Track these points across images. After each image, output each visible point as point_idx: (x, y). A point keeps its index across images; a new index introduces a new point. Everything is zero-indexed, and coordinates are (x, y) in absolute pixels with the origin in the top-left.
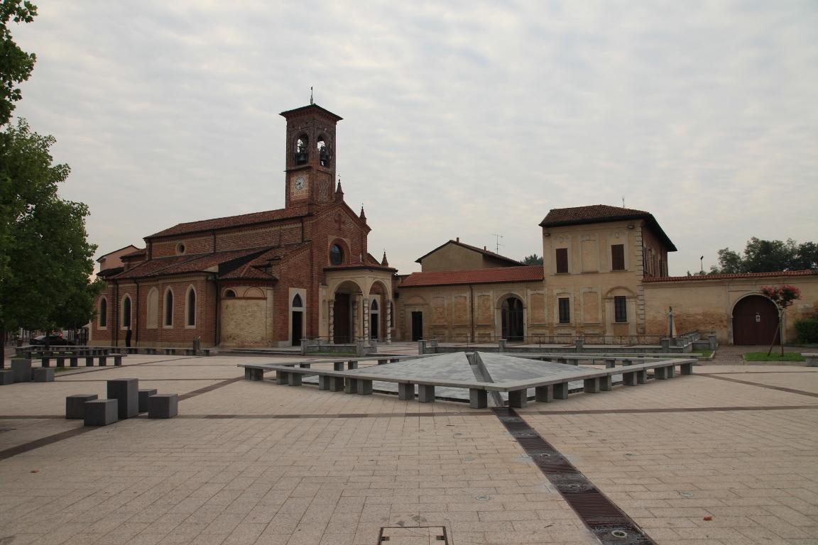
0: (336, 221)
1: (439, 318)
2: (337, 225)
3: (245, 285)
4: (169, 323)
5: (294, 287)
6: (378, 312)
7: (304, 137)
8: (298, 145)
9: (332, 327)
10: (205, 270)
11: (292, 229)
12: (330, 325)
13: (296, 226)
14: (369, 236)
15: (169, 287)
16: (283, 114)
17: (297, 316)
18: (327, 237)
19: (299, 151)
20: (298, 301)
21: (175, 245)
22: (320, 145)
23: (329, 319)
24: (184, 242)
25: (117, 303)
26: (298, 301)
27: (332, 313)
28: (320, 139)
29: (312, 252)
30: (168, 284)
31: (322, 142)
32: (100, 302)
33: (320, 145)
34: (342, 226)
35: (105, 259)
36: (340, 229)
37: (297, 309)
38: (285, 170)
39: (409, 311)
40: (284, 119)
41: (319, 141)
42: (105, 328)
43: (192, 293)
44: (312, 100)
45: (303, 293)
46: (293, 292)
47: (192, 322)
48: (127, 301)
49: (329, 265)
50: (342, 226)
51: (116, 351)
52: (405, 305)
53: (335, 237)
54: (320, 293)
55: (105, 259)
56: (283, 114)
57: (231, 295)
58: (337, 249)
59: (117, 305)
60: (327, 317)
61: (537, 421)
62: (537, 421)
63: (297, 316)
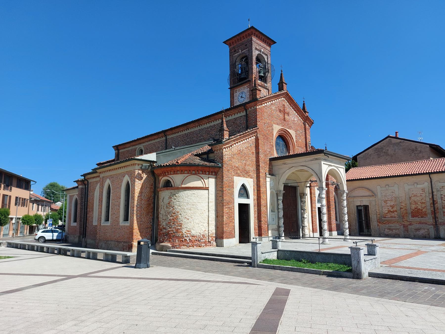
0: (280, 111)
1: (389, 211)
2: (281, 116)
3: (182, 172)
4: (107, 219)
5: (239, 176)
6: (251, 201)
9: (282, 221)
10: (139, 157)
11: (235, 119)
12: (279, 218)
13: (239, 115)
17: (244, 209)
18: (272, 126)
20: (244, 191)
21: (135, 150)
23: (278, 212)
26: (244, 191)
27: (281, 206)
29: (257, 140)
30: (107, 177)
36: (284, 119)
37: (244, 201)
42: (75, 224)
45: (250, 184)
46: (238, 182)
47: (107, 219)
49: (276, 155)
51: (91, 255)
53: (280, 127)
57: (168, 185)
60: (276, 211)
63: (244, 209)
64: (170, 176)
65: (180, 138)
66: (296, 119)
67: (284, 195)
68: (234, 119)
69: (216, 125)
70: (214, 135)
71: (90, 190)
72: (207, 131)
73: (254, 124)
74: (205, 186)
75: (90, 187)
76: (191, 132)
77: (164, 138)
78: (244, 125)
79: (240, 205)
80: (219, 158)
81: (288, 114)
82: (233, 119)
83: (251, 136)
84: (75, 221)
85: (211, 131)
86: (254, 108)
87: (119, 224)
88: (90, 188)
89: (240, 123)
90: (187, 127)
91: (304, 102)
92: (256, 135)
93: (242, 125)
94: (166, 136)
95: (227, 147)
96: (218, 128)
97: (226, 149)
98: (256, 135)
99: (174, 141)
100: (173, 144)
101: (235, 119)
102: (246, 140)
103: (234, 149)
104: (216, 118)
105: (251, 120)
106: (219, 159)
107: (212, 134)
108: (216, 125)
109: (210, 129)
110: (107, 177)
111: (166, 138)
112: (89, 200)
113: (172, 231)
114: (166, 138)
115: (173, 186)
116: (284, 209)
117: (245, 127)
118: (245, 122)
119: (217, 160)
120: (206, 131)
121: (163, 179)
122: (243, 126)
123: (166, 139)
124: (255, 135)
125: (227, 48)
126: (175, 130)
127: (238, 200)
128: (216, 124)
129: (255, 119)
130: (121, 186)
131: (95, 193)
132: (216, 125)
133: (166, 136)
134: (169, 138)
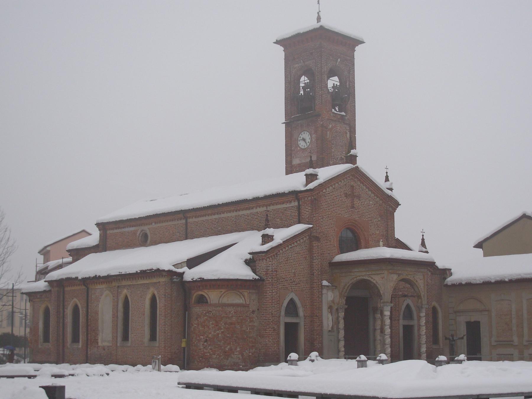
0: (346, 195)
7: (308, 72)
8: (302, 85)
11: (286, 209)
14: (398, 214)
15: (125, 291)
16: (277, 42)
19: (302, 92)
22: (333, 82)
23: (339, 332)
24: (146, 228)
25: (64, 311)
28: (332, 73)
30: (125, 286)
31: (336, 78)
32: (149, 297)
33: (333, 82)
34: (356, 201)
35: (49, 251)
38: (284, 121)
39: (462, 319)
40: (280, 49)
41: (328, 78)
43: (153, 300)
44: (319, 19)
48: (76, 310)
50: (356, 201)
52: (455, 312)
54: (324, 296)
55: (49, 252)
56: (277, 42)
58: (350, 235)
59: (64, 315)
61: (6, 295)
62: (6, 295)
64: (206, 291)
65: (208, 224)
66: (371, 202)
67: (346, 311)
68: (283, 208)
69: (259, 212)
70: (256, 226)
71: (91, 299)
72: (246, 219)
73: (307, 220)
74: (244, 303)
75: (91, 295)
76: (224, 217)
77: (184, 221)
78: (295, 219)
79: (286, 324)
80: (261, 269)
81: (359, 197)
82: (281, 208)
83: (300, 239)
84: (46, 339)
85: (253, 221)
86: (308, 199)
87: (144, 345)
88: (91, 296)
89: (291, 215)
90: (218, 210)
91: (387, 173)
92: (309, 235)
93: (294, 219)
94: (186, 218)
95: (271, 256)
96: (262, 217)
97: (271, 259)
98: (309, 235)
99: (199, 227)
100: (197, 231)
101: (285, 209)
102: (294, 244)
103: (280, 256)
104: (259, 203)
105: (304, 214)
106: (261, 271)
107: (254, 225)
108: (259, 212)
109: (251, 218)
110: (125, 286)
111: (186, 221)
112: (90, 313)
113: (209, 353)
114: (186, 221)
115: (209, 301)
116: (346, 329)
117: (297, 222)
118: (296, 214)
119: (259, 272)
120: (245, 219)
121: (195, 295)
122: (295, 220)
123: (186, 223)
124: (308, 235)
125: (280, 51)
126: (200, 212)
127: (284, 319)
128: (260, 212)
129: (308, 213)
130: (144, 299)
131: (100, 304)
132: (259, 214)
133: (186, 218)
134: (190, 222)
